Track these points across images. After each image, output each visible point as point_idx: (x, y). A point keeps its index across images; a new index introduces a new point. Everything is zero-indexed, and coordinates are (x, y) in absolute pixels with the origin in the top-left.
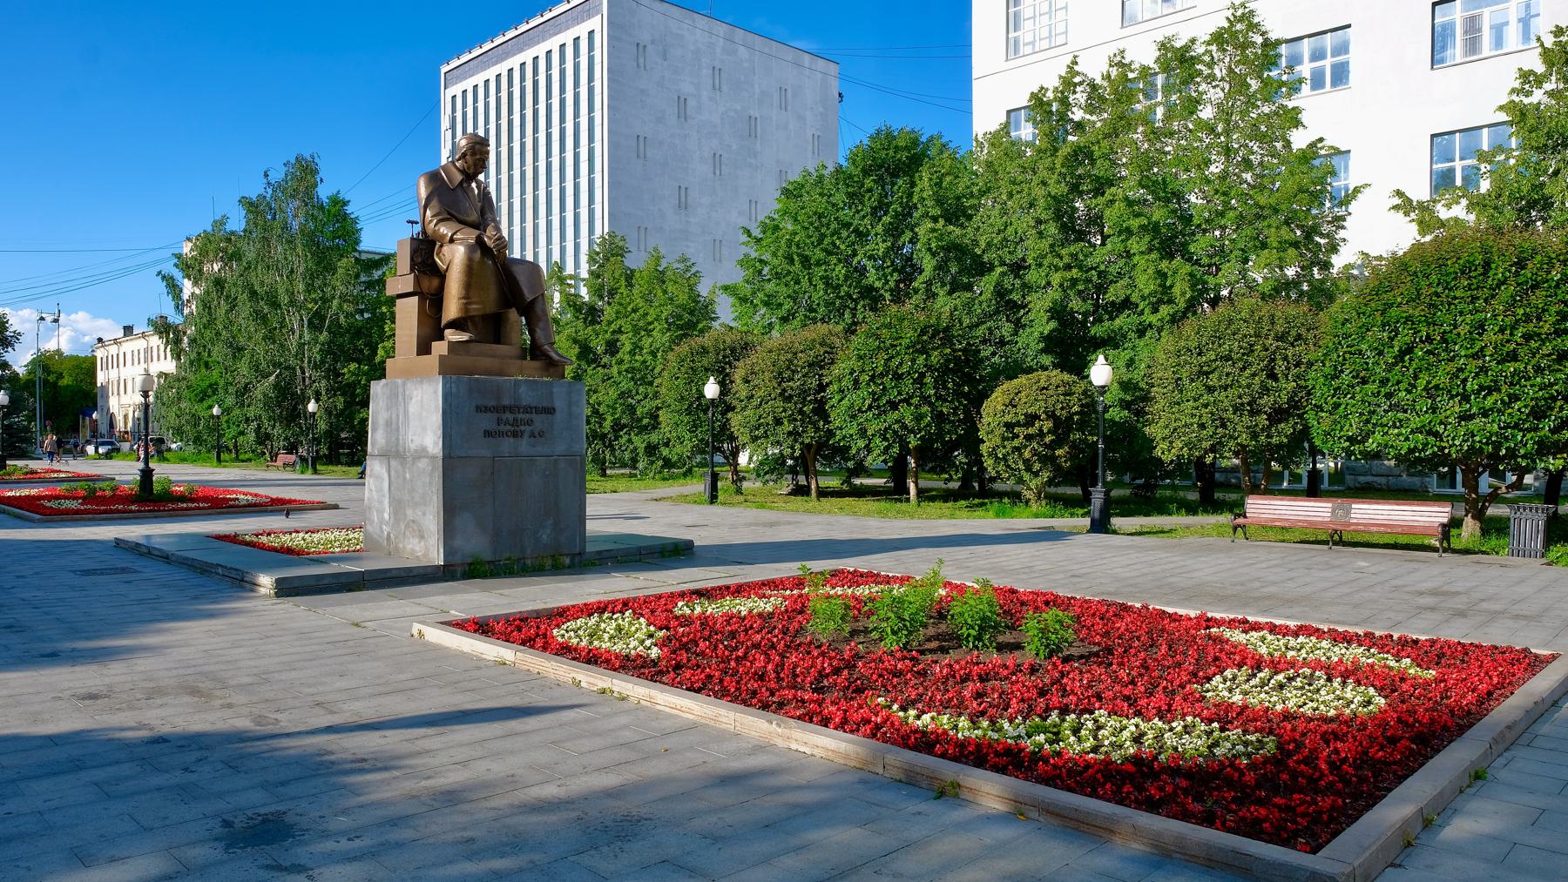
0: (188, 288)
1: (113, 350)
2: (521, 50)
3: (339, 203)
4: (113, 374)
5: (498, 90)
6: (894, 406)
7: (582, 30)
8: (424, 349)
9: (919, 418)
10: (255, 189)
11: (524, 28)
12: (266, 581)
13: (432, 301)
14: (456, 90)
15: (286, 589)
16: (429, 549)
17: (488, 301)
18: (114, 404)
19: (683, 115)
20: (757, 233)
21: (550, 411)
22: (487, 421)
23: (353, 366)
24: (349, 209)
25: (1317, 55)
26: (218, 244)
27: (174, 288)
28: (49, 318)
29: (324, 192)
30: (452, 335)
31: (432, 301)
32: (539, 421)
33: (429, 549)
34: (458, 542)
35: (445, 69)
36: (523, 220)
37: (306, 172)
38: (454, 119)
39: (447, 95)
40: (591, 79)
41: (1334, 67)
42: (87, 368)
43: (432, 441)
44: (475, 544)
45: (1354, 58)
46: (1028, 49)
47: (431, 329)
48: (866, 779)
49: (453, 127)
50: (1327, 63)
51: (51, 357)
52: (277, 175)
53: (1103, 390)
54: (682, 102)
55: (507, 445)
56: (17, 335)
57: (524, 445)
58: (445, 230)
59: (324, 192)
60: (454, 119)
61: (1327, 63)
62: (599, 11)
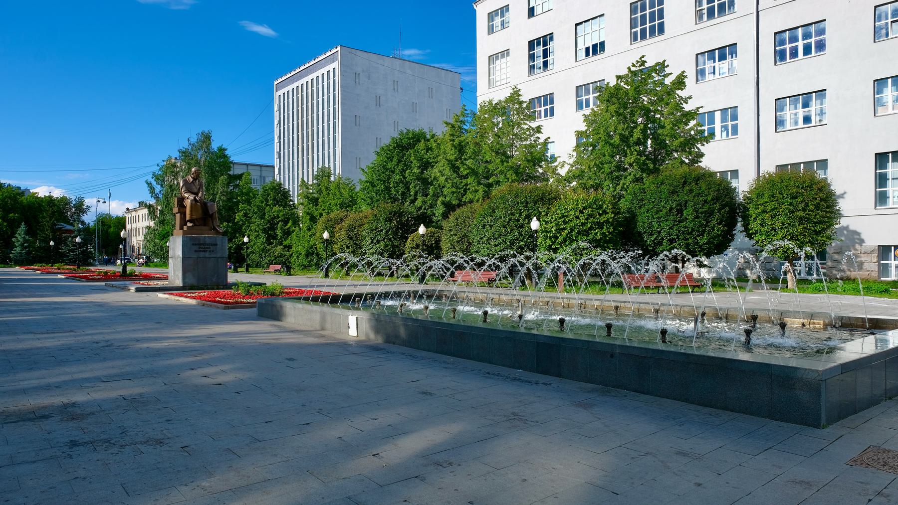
0: (158, 188)
1: (134, 214)
2: (307, 76)
3: (222, 150)
4: (134, 226)
5: (302, 91)
6: (378, 241)
7: (330, 68)
8: (181, 228)
9: (386, 246)
10: (185, 145)
11: (307, 65)
12: (133, 288)
13: (183, 214)
14: (280, 92)
15: (138, 290)
16: (179, 282)
17: (199, 214)
18: (134, 241)
19: (378, 103)
20: (366, 170)
21: (216, 245)
22: (196, 248)
23: (225, 224)
24: (227, 152)
25: (807, 36)
26: (170, 169)
27: (152, 190)
28: (102, 201)
29: (215, 146)
30: (189, 224)
31: (183, 214)
32: (212, 248)
33: (179, 282)
34: (187, 280)
35: (276, 83)
36: (308, 154)
37: (206, 138)
38: (279, 106)
39: (277, 94)
40: (334, 90)
41: (816, 42)
42: (121, 223)
43: (181, 255)
44: (191, 281)
45: (827, 36)
46: (498, 84)
47: (183, 222)
48: (198, 305)
49: (279, 110)
50: (813, 40)
51: (105, 218)
52: (194, 140)
53: (536, 231)
54: (378, 99)
55: (202, 254)
56: (88, 208)
57: (207, 255)
58: (186, 195)
59: (215, 146)
60: (279, 106)
61: (813, 40)
62: (337, 59)
